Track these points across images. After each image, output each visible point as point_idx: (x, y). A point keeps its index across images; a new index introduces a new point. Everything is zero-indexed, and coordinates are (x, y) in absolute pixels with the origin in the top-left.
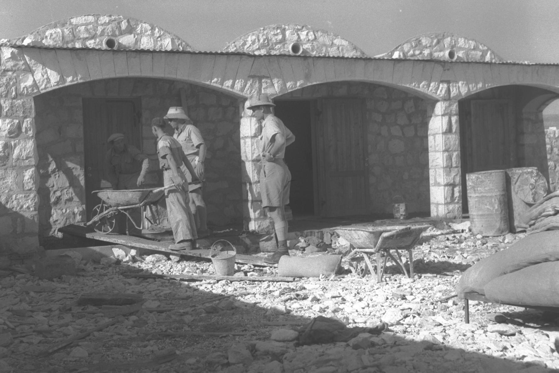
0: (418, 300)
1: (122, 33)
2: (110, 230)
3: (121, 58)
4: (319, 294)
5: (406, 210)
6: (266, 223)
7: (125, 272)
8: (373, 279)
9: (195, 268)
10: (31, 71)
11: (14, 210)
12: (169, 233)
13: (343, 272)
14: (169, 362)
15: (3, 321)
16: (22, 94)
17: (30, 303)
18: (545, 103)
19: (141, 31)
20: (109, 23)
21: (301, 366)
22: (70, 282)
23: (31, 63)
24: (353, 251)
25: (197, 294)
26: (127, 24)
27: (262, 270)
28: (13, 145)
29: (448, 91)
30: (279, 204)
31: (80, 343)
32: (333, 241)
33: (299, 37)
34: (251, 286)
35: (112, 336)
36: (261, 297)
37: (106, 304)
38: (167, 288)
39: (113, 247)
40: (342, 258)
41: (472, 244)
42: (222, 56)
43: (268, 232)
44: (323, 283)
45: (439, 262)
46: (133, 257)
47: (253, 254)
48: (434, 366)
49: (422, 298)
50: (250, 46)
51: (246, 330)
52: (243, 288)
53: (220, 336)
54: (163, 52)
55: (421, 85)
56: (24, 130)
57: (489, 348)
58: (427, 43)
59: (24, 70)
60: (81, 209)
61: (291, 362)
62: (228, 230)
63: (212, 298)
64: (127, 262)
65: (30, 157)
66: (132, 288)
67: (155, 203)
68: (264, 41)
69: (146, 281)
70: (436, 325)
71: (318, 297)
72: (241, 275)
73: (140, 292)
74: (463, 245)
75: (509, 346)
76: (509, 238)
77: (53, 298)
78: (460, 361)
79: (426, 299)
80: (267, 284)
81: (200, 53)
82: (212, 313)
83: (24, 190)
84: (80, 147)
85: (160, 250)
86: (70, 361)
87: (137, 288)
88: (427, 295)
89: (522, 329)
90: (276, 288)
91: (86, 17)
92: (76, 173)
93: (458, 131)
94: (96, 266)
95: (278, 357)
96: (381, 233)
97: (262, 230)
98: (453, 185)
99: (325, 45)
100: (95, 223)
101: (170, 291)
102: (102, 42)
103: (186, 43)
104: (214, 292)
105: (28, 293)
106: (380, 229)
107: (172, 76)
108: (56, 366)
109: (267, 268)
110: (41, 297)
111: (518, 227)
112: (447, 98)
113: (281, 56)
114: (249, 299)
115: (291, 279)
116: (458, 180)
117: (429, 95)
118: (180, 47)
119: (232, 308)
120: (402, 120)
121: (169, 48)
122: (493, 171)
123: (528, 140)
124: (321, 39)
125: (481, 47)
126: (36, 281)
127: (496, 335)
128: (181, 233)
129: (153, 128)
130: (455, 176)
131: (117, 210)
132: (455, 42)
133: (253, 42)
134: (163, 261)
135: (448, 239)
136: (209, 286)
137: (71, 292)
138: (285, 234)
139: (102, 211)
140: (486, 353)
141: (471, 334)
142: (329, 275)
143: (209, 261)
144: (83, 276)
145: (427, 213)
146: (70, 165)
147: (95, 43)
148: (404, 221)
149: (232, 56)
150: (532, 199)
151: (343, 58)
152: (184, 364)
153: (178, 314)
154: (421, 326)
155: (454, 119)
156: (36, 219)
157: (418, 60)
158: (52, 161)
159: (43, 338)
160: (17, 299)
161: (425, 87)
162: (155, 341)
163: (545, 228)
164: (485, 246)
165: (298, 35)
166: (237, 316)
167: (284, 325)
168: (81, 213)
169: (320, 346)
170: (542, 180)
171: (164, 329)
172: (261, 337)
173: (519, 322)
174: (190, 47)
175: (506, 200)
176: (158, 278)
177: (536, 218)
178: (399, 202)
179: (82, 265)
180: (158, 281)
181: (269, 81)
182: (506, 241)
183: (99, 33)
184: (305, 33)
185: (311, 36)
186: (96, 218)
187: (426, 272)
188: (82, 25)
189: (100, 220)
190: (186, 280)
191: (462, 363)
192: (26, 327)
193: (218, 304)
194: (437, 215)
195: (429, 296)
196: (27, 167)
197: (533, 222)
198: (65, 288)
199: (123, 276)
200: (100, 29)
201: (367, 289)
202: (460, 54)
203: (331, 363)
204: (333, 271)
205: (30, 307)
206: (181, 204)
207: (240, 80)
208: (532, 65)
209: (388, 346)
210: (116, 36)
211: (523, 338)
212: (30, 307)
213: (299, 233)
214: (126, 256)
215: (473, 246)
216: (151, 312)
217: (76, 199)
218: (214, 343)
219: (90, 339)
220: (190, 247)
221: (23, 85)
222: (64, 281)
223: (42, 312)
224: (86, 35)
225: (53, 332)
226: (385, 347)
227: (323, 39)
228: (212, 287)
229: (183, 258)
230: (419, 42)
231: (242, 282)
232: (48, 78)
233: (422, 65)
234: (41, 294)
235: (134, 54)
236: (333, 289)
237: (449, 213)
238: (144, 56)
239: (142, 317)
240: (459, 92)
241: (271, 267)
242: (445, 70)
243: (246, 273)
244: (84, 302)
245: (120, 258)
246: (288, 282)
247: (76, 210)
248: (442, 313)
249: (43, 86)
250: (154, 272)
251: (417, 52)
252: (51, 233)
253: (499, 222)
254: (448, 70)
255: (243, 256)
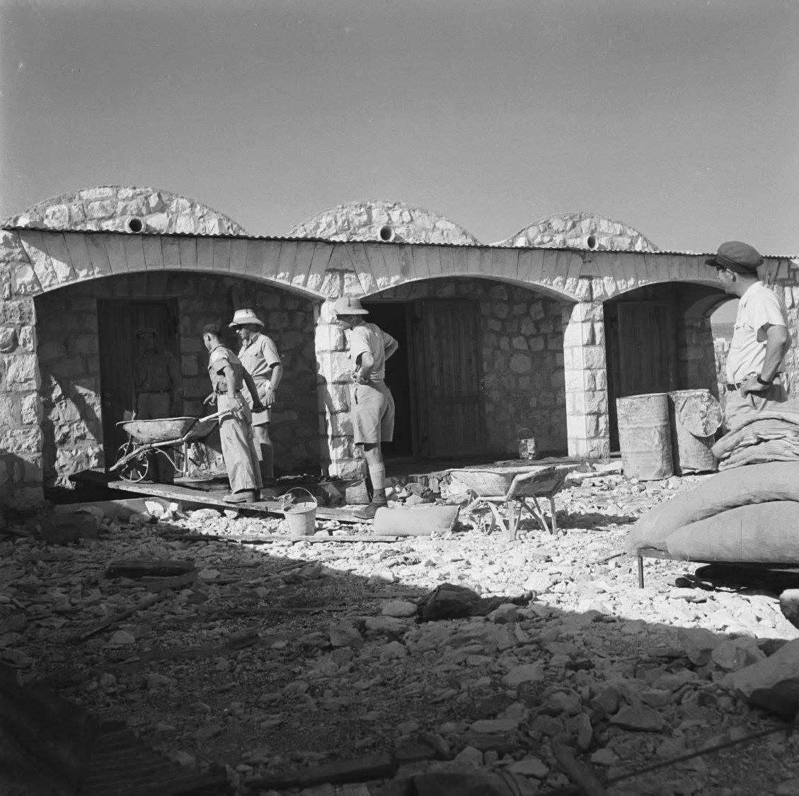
0: (568, 562)
1: (150, 212)
2: (142, 477)
3: (155, 244)
4: (434, 557)
5: (536, 447)
6: (354, 465)
7: (165, 533)
8: (504, 536)
9: (261, 526)
10: (30, 262)
11: (9, 451)
12: (224, 481)
13: (461, 529)
14: (248, 646)
15: (9, 600)
16: (18, 294)
17: (40, 576)
18: (713, 306)
19: (177, 208)
20: (133, 198)
21: (433, 646)
22: (91, 547)
23: (31, 251)
24: (475, 501)
25: (267, 560)
26: (157, 199)
27: (352, 528)
28: (6, 362)
29: (591, 289)
30: (376, 439)
31: (121, 626)
32: (442, 489)
33: (390, 219)
34: (339, 548)
35: (162, 616)
36: (357, 562)
37: (147, 575)
38: (225, 554)
39: (146, 500)
40: (459, 509)
41: (626, 490)
42: (290, 244)
43: (354, 477)
44: (436, 543)
45: (586, 514)
46: (174, 513)
47: (336, 507)
48: (611, 641)
49: (573, 559)
50: (325, 229)
51: (344, 604)
52: (329, 551)
53: (311, 613)
54: (211, 237)
55: (554, 282)
56: (21, 342)
57: (676, 618)
58: (559, 226)
59: (21, 261)
60: (97, 450)
61: (416, 642)
62: (299, 476)
63: (290, 565)
64: (166, 520)
65: (31, 379)
66: (178, 554)
67: (202, 439)
68: (344, 223)
69: (195, 544)
70: (598, 592)
71: (434, 561)
72: (324, 534)
73: (189, 559)
74: (614, 492)
75: (701, 616)
76: (674, 481)
77: (71, 569)
78: (643, 635)
79: (578, 560)
80: (362, 546)
81: (261, 238)
82: (294, 583)
83: (22, 424)
84: (95, 366)
85: (211, 503)
86: (112, 649)
87: (185, 554)
88: (578, 555)
89: (713, 593)
90: (376, 550)
91: (102, 189)
92: (89, 401)
93: (603, 342)
94: (125, 526)
95: (395, 636)
96: (514, 475)
97: (346, 475)
98: (598, 414)
99: (424, 229)
100: (121, 467)
101: (231, 557)
102: (123, 223)
103: (238, 226)
104: (291, 557)
105: (35, 563)
106: (515, 470)
107: (224, 270)
108: (95, 656)
109: (359, 525)
110: (53, 567)
111: (684, 468)
112: (589, 300)
113: (370, 243)
114: (341, 566)
115: (393, 539)
116: (604, 407)
117: (565, 296)
118: (230, 230)
119: (320, 577)
120: (527, 329)
121: (217, 232)
122: (652, 395)
123: (692, 354)
124: (419, 222)
125: (629, 232)
126: (43, 546)
127: (682, 603)
128: (240, 480)
129: (206, 338)
130: (599, 402)
131: (151, 448)
132: (595, 225)
133: (329, 225)
134: (215, 518)
135: (594, 485)
136: (282, 550)
137: (95, 560)
138: (383, 481)
139: (130, 450)
140: (673, 624)
141: (650, 602)
142: (443, 533)
143: (281, 516)
144: (107, 539)
145: (565, 452)
146: (82, 390)
147: (113, 225)
148: (533, 462)
149: (304, 243)
150: (702, 431)
151: (451, 246)
152: (269, 649)
153: (246, 585)
154: (577, 594)
155: (599, 326)
156: (39, 464)
157: (551, 249)
158: (56, 385)
159: (68, 621)
160: (22, 571)
161: (560, 284)
162: (223, 621)
163: (744, 462)
164: (643, 492)
165: (389, 215)
166: (329, 587)
167: (394, 597)
168: (98, 456)
169: (450, 622)
170: (716, 405)
171: (232, 605)
172: (366, 612)
173: (707, 585)
174: (244, 230)
175: (669, 432)
176: (212, 540)
177: (732, 449)
178: (527, 437)
179: (105, 525)
180: (212, 545)
181: (353, 276)
182: (670, 487)
183: (119, 211)
184: (398, 212)
185: (406, 218)
186: (122, 461)
187: (572, 527)
188: (96, 200)
189: (128, 463)
190: (249, 543)
191: (646, 636)
192: (41, 607)
193: (300, 572)
194: (577, 454)
195: (582, 556)
196: (28, 392)
197: (726, 454)
198: (85, 556)
199: (164, 538)
200: (121, 205)
201: (496, 550)
202: (601, 242)
203: (473, 641)
204: (448, 527)
205: (41, 581)
206: (242, 444)
207: (315, 275)
208: (699, 255)
209: (541, 619)
210: (142, 215)
211: (717, 604)
212: (41, 581)
213: (395, 479)
214: (165, 511)
215: (628, 493)
216: (210, 584)
217: (90, 436)
218: (304, 622)
219: (133, 620)
220: (251, 499)
221: (19, 281)
222: (83, 547)
223: (59, 586)
224: (101, 215)
225: (80, 613)
226: (537, 621)
227: (422, 221)
228: (286, 551)
229: (243, 513)
230: (548, 225)
231: (327, 544)
232: (54, 272)
233: (555, 255)
234: (54, 563)
235: (170, 240)
236: (451, 550)
237: (592, 450)
238: (185, 242)
239: (200, 590)
240: (605, 291)
241: (363, 524)
242: (585, 262)
243: (330, 532)
244: (117, 572)
245: (156, 515)
246: (389, 542)
247: (90, 452)
248: (602, 577)
249: (47, 283)
250: (204, 533)
251: (546, 239)
252: (56, 482)
253: (660, 462)
254: (590, 262)
255: (325, 510)
